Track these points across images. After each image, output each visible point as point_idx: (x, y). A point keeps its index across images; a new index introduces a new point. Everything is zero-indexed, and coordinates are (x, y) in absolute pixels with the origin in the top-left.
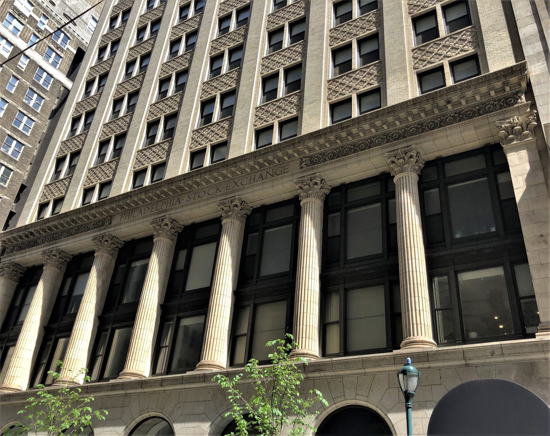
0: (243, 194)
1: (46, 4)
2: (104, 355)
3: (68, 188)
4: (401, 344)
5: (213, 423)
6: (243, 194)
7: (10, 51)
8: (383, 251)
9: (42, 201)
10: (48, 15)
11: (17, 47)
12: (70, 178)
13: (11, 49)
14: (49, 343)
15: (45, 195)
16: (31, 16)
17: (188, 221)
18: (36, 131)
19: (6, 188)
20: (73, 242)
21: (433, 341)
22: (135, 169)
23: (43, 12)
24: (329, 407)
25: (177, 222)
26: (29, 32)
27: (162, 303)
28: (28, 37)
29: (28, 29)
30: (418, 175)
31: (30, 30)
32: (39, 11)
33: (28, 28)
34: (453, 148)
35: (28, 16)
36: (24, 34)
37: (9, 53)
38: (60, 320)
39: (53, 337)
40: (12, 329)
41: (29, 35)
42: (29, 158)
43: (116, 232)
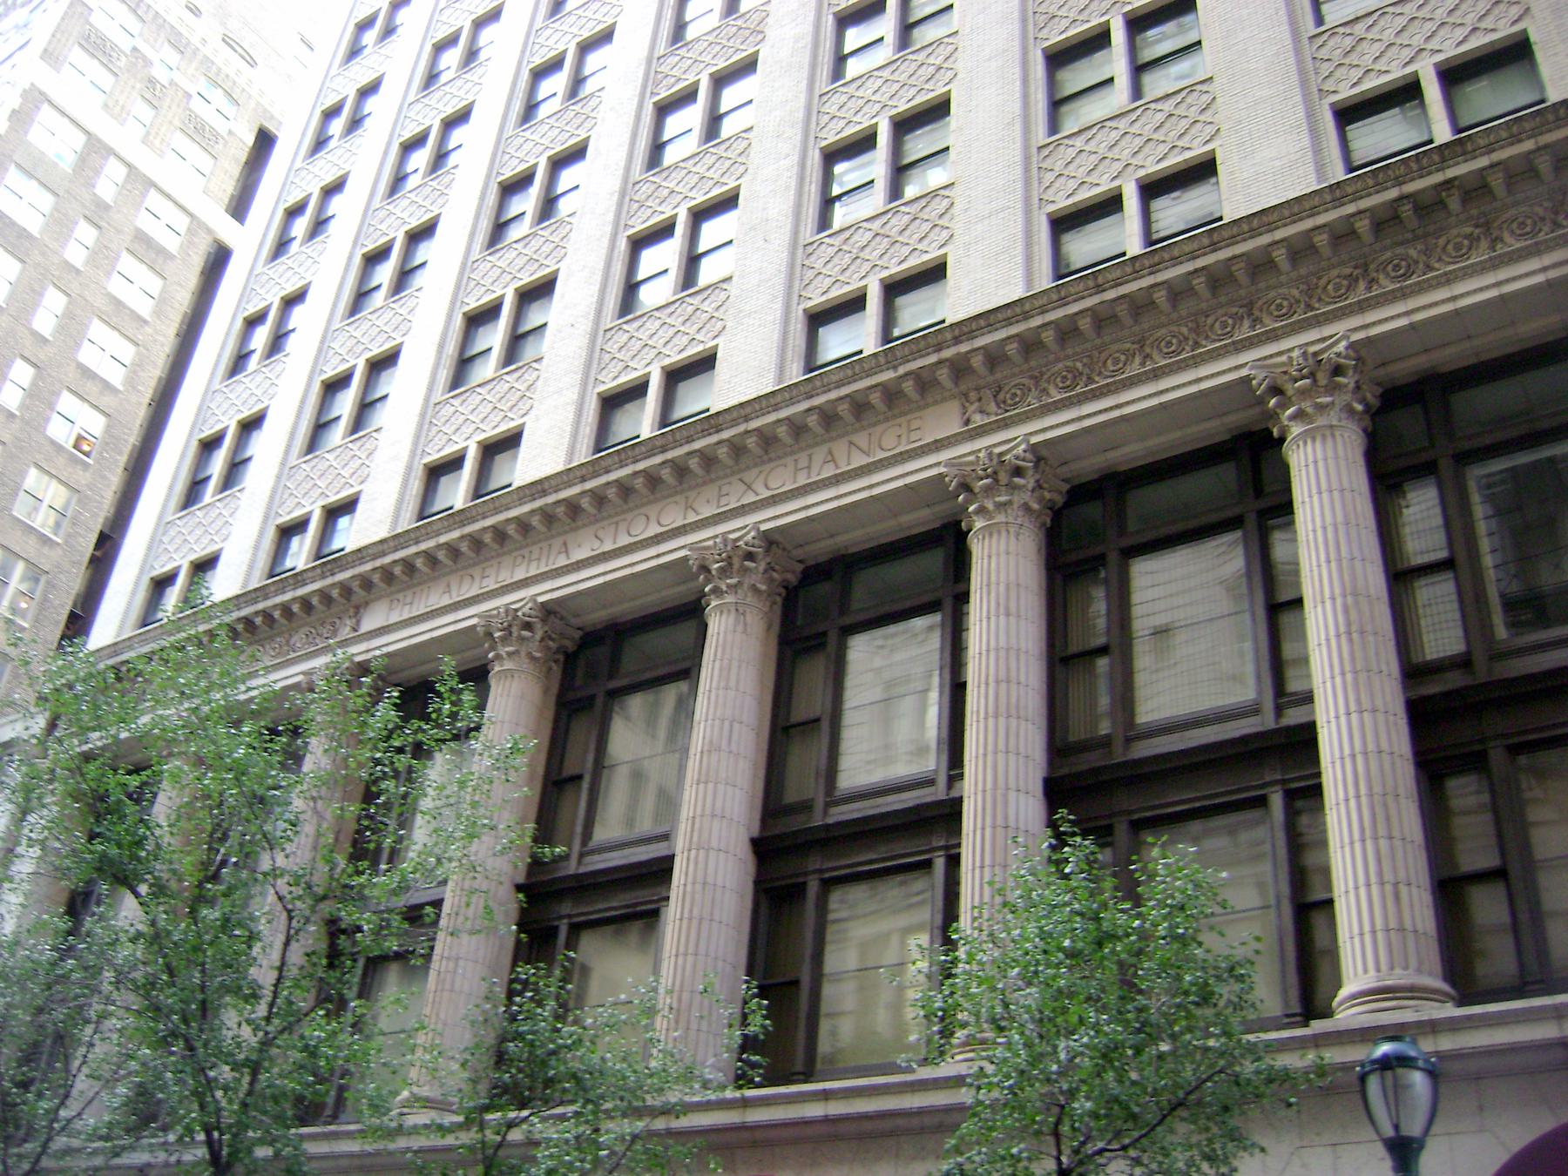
1: (175, 14)
4: (1337, 1000)
8: (1260, 692)
16: (135, 49)
17: (822, 544)
18: (141, 374)
19: (58, 544)
21: (1445, 987)
24: (570, 849)
30: (1365, 430)
34: (1476, 342)
35: (127, 49)
42: (120, 453)
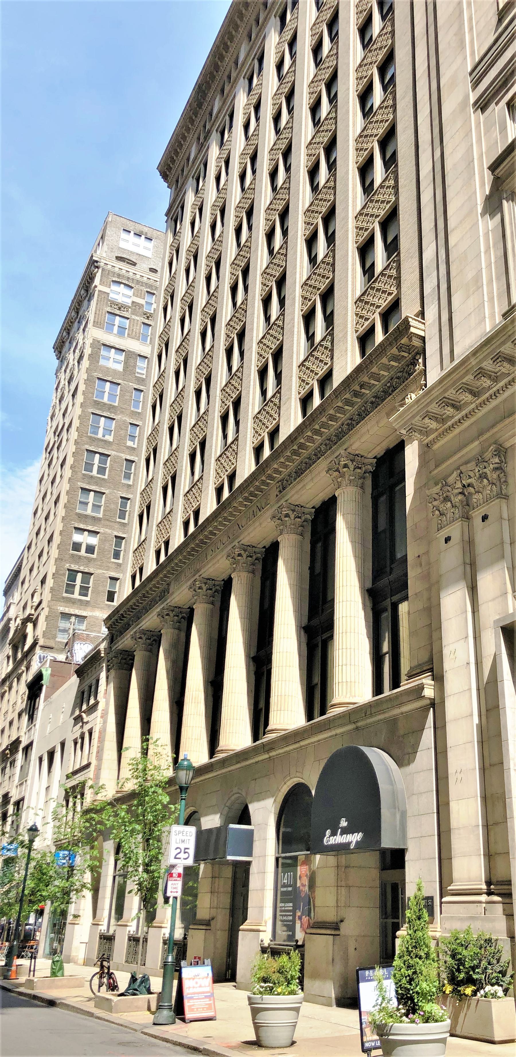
0: (291, 497)
2: (391, 652)
3: (332, 350)
5: (221, 814)
6: (291, 497)
7: (123, 360)
9: (361, 330)
10: (152, 289)
11: (129, 351)
12: (331, 334)
13: (122, 357)
14: (384, 615)
15: (303, 381)
20: (213, 565)
22: (359, 333)
23: (146, 290)
25: (362, 457)
26: (137, 324)
27: (305, 621)
28: (138, 331)
29: (136, 321)
31: (138, 320)
32: (141, 290)
33: (134, 320)
36: (133, 330)
37: (123, 363)
38: (320, 612)
39: (387, 603)
40: (323, 610)
41: (138, 328)
43: (173, 601)
